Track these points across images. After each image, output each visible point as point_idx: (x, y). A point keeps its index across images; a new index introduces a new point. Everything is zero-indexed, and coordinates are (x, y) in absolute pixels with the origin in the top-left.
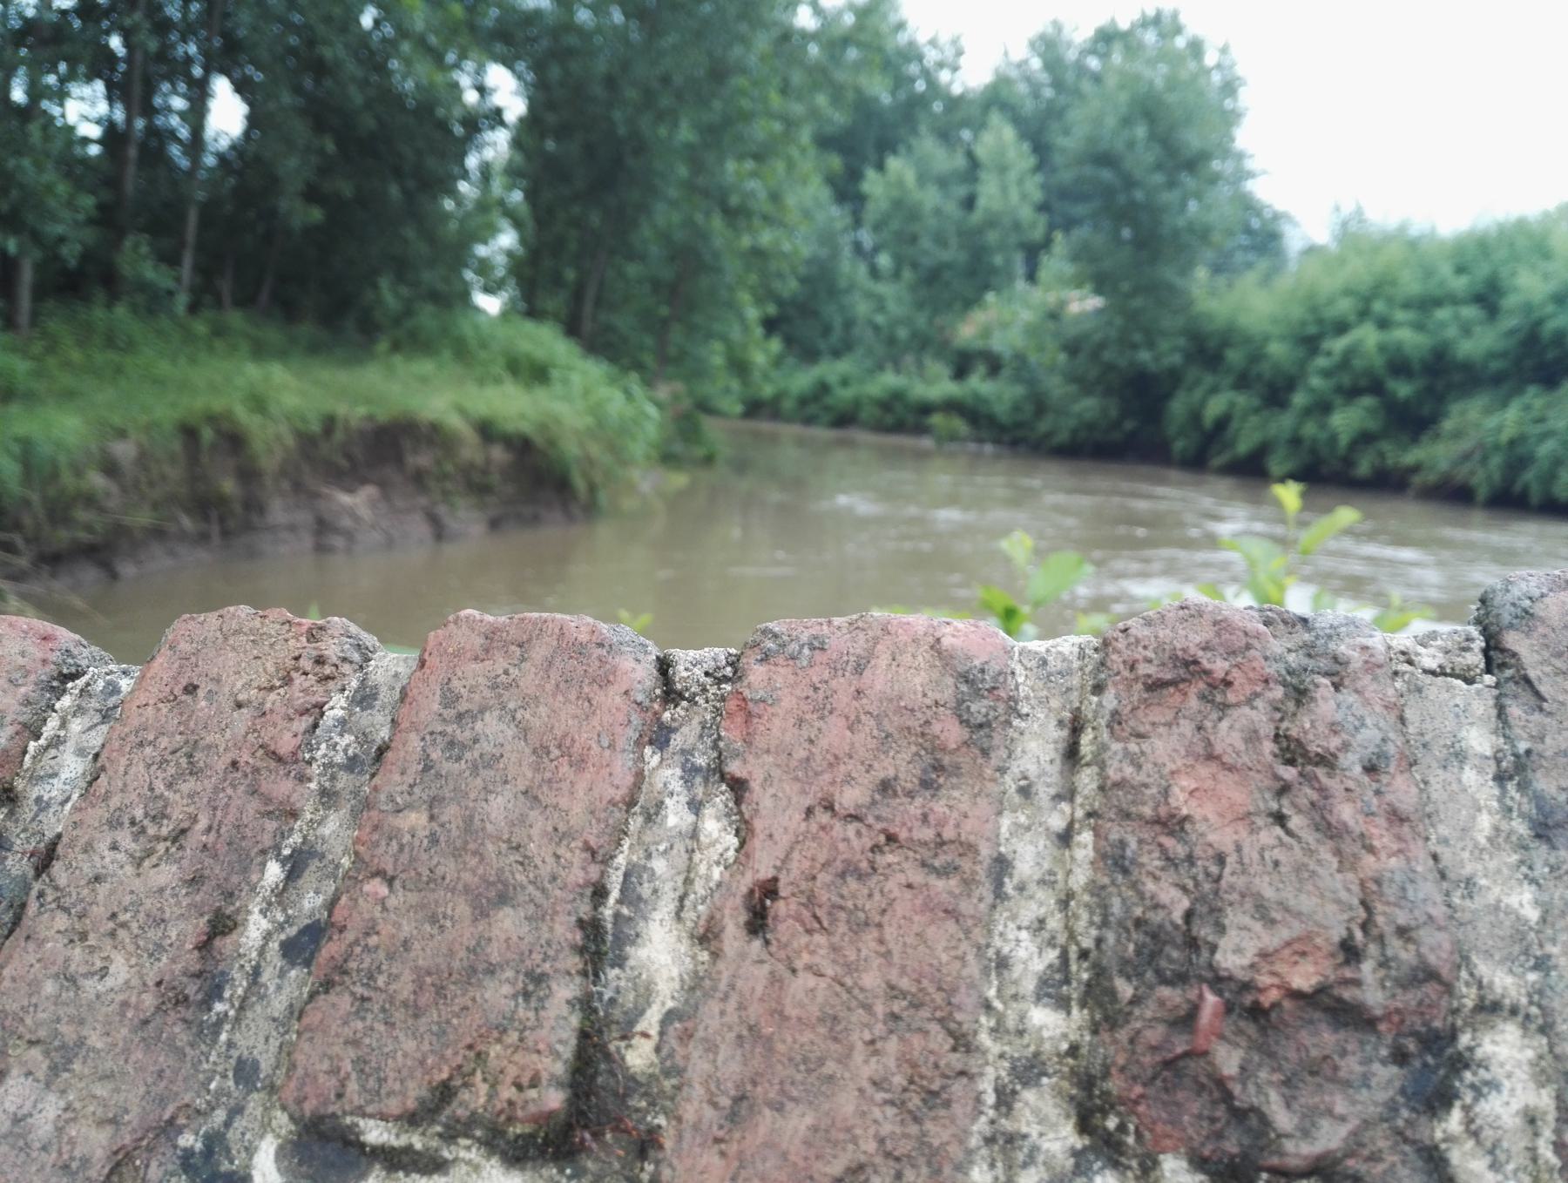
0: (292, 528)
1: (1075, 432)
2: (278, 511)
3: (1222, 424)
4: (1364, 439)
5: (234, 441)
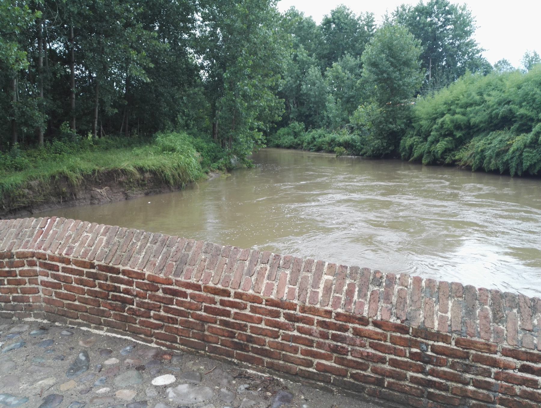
0: (85, 199)
1: (373, 151)
2: (81, 195)
3: (411, 147)
4: (447, 151)
5: (66, 178)
